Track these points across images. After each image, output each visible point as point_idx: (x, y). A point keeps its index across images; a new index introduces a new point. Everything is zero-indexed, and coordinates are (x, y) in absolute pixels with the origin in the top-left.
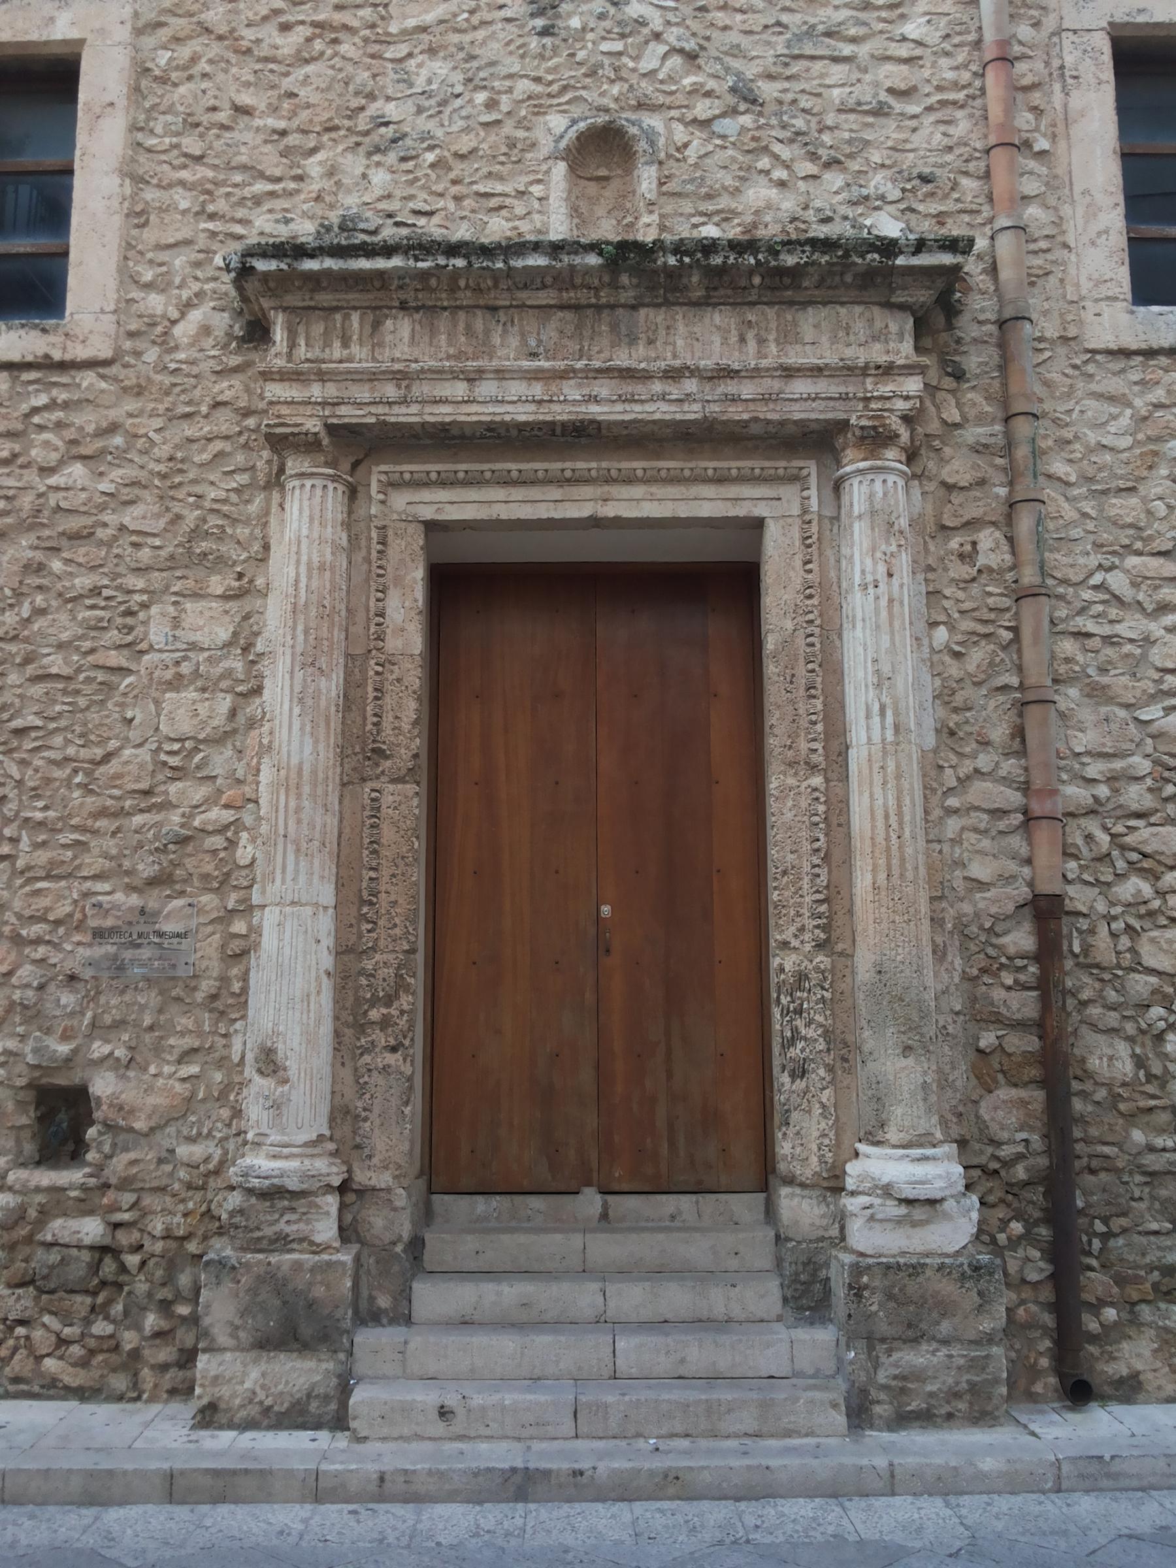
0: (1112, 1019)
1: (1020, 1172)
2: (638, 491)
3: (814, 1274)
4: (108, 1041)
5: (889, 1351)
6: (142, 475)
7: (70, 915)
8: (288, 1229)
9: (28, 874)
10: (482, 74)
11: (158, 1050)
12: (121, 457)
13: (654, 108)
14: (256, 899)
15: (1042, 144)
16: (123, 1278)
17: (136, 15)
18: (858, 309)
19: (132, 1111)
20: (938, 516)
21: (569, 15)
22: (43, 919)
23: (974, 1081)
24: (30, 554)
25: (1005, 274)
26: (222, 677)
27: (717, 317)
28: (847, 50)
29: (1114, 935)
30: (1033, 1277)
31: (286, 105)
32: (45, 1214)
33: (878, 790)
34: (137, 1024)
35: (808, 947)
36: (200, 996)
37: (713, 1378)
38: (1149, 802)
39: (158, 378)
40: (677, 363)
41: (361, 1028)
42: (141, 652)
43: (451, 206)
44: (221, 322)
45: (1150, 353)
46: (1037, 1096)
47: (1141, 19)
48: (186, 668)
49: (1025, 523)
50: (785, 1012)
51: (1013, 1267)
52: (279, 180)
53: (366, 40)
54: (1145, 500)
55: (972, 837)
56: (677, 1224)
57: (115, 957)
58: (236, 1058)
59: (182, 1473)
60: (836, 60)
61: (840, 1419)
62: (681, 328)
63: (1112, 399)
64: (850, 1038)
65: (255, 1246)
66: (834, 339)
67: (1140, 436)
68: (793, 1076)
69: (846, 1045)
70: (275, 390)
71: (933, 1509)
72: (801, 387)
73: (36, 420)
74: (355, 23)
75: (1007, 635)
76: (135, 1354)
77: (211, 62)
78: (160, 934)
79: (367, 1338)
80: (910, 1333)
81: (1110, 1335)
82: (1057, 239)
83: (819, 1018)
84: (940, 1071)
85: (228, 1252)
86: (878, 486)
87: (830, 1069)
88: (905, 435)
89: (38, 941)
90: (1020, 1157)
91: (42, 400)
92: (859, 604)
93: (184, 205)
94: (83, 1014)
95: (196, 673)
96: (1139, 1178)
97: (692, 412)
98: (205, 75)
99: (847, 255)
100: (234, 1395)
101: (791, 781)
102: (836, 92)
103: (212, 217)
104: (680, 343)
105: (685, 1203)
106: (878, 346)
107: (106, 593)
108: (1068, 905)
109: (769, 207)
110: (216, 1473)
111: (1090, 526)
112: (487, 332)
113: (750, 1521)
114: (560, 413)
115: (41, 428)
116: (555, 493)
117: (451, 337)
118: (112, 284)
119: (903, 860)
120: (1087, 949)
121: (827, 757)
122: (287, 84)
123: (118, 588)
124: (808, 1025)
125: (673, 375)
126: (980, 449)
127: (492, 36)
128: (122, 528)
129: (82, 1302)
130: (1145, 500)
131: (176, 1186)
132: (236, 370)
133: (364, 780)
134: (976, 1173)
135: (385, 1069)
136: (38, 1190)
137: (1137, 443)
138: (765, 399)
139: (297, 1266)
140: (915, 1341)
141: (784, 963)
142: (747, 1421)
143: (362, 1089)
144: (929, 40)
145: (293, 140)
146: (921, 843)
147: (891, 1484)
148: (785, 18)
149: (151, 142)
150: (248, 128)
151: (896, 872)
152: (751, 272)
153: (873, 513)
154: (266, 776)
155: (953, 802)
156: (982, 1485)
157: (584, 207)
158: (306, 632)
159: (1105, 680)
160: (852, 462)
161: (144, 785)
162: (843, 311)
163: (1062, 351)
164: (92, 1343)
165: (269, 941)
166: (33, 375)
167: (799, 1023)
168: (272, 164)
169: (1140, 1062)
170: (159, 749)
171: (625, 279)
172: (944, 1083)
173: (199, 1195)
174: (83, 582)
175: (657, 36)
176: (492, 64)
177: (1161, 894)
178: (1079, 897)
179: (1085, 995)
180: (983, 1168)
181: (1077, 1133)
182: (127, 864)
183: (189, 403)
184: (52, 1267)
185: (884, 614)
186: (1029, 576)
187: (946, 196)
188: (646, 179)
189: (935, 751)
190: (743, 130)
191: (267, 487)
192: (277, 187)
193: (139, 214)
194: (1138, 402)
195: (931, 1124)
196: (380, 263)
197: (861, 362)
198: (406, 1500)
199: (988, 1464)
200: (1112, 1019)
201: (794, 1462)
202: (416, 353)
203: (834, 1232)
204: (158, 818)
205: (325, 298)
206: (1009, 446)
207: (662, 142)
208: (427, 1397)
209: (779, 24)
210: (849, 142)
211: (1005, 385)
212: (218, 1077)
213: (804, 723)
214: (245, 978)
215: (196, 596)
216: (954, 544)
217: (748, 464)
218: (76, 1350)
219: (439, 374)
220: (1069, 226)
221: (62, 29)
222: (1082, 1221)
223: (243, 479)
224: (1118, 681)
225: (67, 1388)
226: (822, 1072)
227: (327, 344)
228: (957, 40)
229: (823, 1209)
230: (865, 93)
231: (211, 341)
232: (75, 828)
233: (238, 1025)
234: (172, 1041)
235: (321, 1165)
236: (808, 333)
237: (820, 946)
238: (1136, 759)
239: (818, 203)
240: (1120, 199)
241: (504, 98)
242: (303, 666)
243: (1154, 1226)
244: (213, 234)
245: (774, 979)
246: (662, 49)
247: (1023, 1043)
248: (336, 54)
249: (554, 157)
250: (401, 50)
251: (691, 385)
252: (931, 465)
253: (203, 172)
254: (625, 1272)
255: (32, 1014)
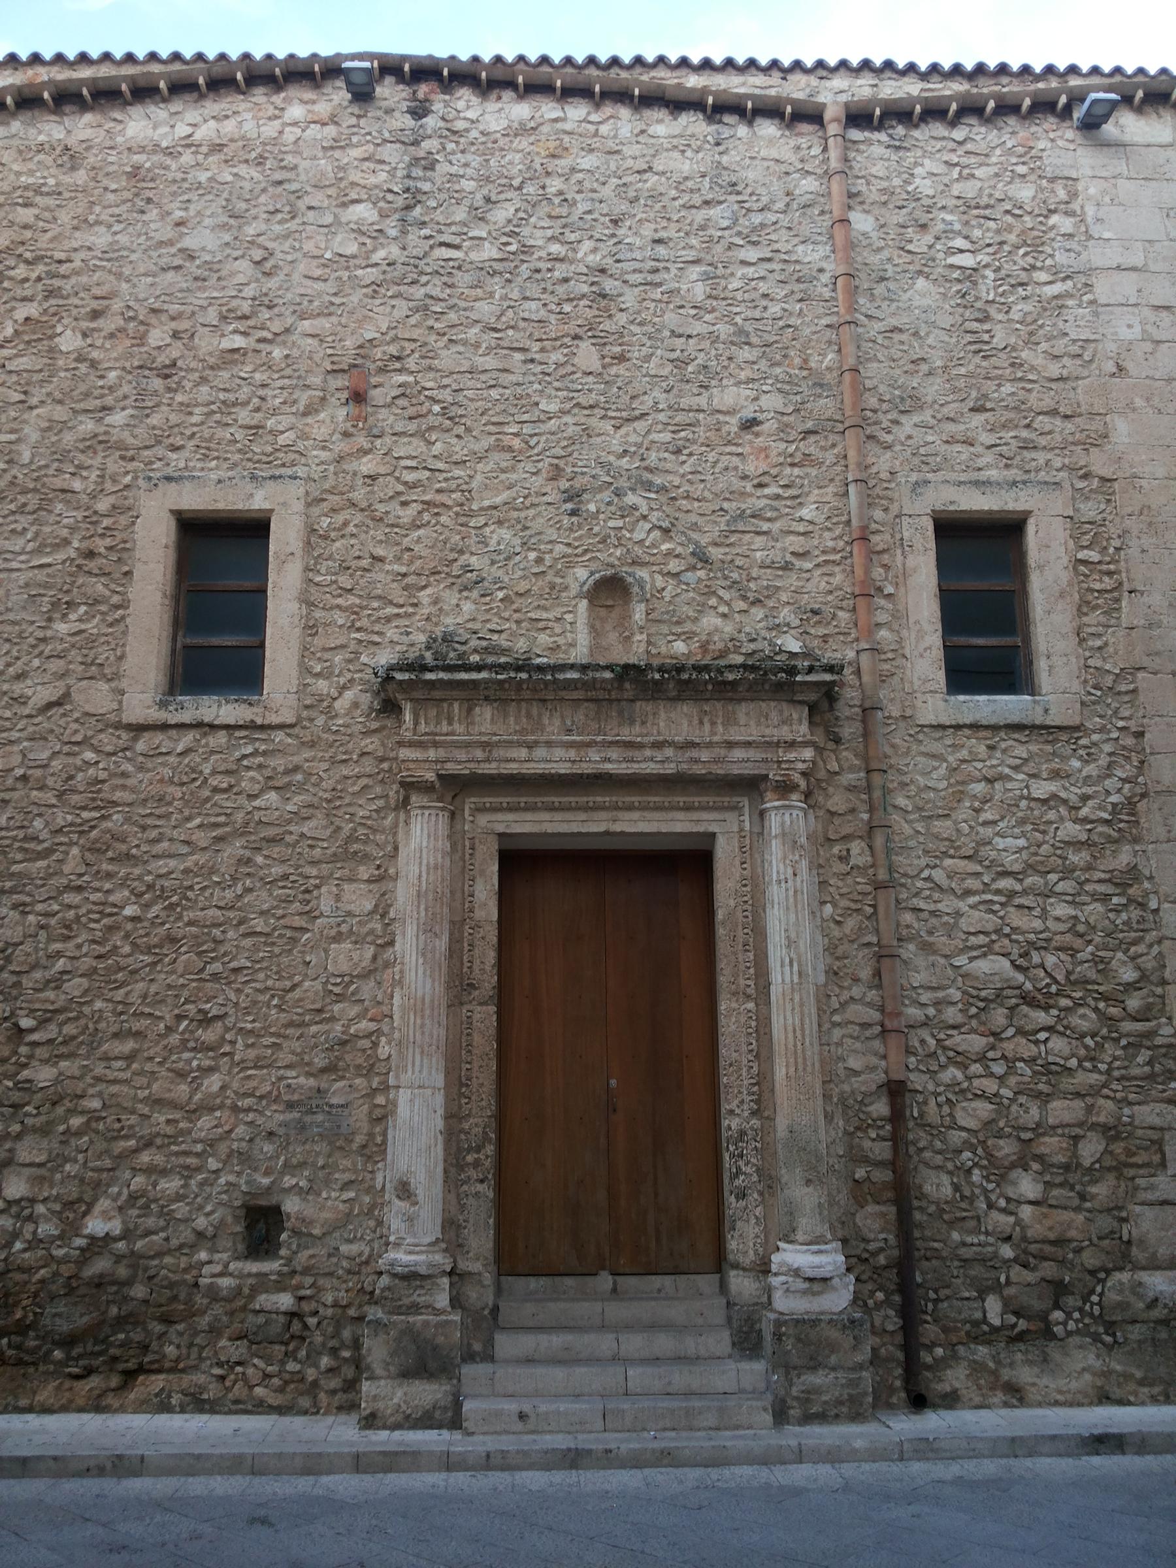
0: (939, 1159)
1: (882, 1260)
2: (635, 815)
3: (752, 1326)
4: (293, 1176)
5: (799, 1376)
6: (315, 800)
7: (270, 1093)
8: (419, 1300)
9: (243, 1065)
10: (533, 540)
11: (327, 1182)
12: (301, 788)
13: (644, 564)
14: (392, 1082)
15: (889, 589)
16: (306, 1333)
17: (307, 493)
18: (773, 704)
19: (311, 1222)
20: (826, 832)
21: (588, 502)
22: (252, 1095)
23: (852, 1201)
24: (242, 852)
25: (866, 678)
26: (368, 934)
27: (686, 708)
28: (765, 526)
29: (939, 1105)
30: (890, 1328)
31: (406, 556)
32: (254, 1291)
33: (789, 1013)
34: (314, 1164)
35: (746, 1114)
36: (355, 1146)
37: (689, 1394)
38: (960, 1019)
39: (325, 736)
40: (661, 738)
41: (461, 1168)
42: (316, 917)
43: (514, 627)
44: (366, 699)
45: (958, 727)
46: (893, 1209)
47: (952, 508)
48: (344, 928)
49: (879, 841)
50: (732, 1156)
51: (877, 1322)
52: (402, 606)
53: (457, 514)
54: (956, 823)
55: (849, 1041)
56: (662, 1295)
57: (300, 1121)
58: (379, 1187)
59: (364, 1454)
60: (758, 533)
61: (768, 1418)
62: (663, 715)
63: (934, 756)
64: (773, 1173)
65: (398, 1311)
66: (758, 724)
67: (952, 781)
68: (737, 1198)
69: (771, 1178)
70: (404, 753)
71: (825, 1470)
72: (738, 754)
73: (245, 763)
74: (450, 503)
75: (869, 910)
76: (315, 1384)
77: (356, 526)
78: (331, 1106)
79: (468, 1370)
80: (812, 1364)
81: (940, 1365)
82: (899, 652)
83: (754, 1160)
84: (829, 1195)
85: (380, 1315)
86: (787, 817)
87: (761, 1194)
88: (803, 784)
89: (249, 1110)
90: (882, 1250)
91: (249, 750)
92: (776, 893)
93: (340, 622)
94: (278, 1158)
95: (351, 932)
96: (956, 1263)
97: (670, 769)
98: (353, 535)
99: (765, 674)
100: (386, 1408)
101: (734, 1005)
102: (759, 554)
103: (359, 630)
104: (662, 724)
105: (667, 1281)
106: (786, 728)
107: (292, 878)
108: (910, 1086)
109: (716, 630)
110: (384, 1453)
111: (921, 839)
112: (540, 715)
113: (714, 1477)
114: (586, 769)
115: (248, 768)
116: (582, 816)
117: (517, 718)
118: (295, 673)
119: (805, 1059)
120: (922, 1115)
121: (757, 989)
122: (406, 542)
123: (300, 875)
124: (746, 1164)
125: (658, 745)
126: (851, 789)
127: (539, 514)
128: (302, 835)
129: (279, 1349)
130: (956, 823)
131: (340, 1272)
132: (375, 731)
133: (462, 1004)
134: (854, 1260)
135: (477, 1195)
136: (250, 1275)
137: (950, 785)
138: (716, 761)
139: (426, 1324)
140: (814, 1369)
141: (731, 1124)
142: (711, 1420)
143: (462, 1208)
144: (817, 520)
145: (411, 580)
146: (817, 1048)
147: (800, 1456)
148: (726, 505)
149: (318, 579)
150: (381, 570)
151: (800, 1068)
152: (706, 682)
153: (784, 834)
154: (397, 1001)
155: (837, 1018)
156: (854, 1456)
157: (598, 625)
158: (426, 910)
159: (931, 939)
160: (771, 801)
161: (318, 1006)
162: (763, 705)
163: (902, 724)
164: (287, 1376)
165: (403, 1110)
166: (243, 733)
167: (741, 1163)
168: (398, 595)
169: (956, 1188)
170: (327, 982)
171: (627, 685)
172: (832, 1202)
173: (356, 1278)
174: (277, 870)
175: (645, 517)
176: (540, 533)
177: (969, 1078)
178: (917, 1081)
179: (921, 1145)
180: (859, 1258)
181: (917, 1234)
182: (307, 1058)
183: (345, 753)
184: (259, 1327)
185: (791, 900)
186: (882, 875)
187: (829, 623)
188: (639, 613)
189: (826, 985)
190: (700, 580)
191: (396, 809)
192: (401, 611)
193: (311, 627)
194: (951, 759)
195: (824, 1230)
196: (474, 676)
197: (775, 739)
198: (503, 1469)
199: (858, 1444)
200: (939, 1159)
201: (740, 1444)
202: (495, 729)
203: (765, 1299)
204: (327, 1027)
205: (437, 694)
206: (869, 788)
207: (648, 587)
208: (512, 1407)
209: (722, 509)
210: (767, 588)
211: (866, 747)
212: (367, 1199)
213: (742, 967)
214: (384, 1134)
215: (351, 880)
216: (836, 850)
217: (706, 799)
218: (276, 1381)
219: (510, 744)
220: (907, 644)
221: (258, 500)
222: (921, 1291)
223: (380, 803)
224: (940, 939)
225: (270, 1406)
226: (756, 1195)
227: (438, 723)
228: (835, 520)
229: (757, 1285)
230: (776, 556)
231: (359, 712)
232: (273, 1034)
233: (380, 1165)
234: (337, 1176)
235: (438, 1258)
236: (742, 719)
237: (754, 1113)
238: (951, 991)
239: (747, 629)
240: (939, 626)
241: (547, 556)
242: (425, 932)
243: (967, 1294)
244: (360, 641)
245: (724, 1134)
246: (648, 526)
247: (883, 1176)
248: (438, 523)
249: (579, 596)
250: (481, 521)
251: (669, 752)
252: (820, 799)
253: (353, 600)
254: (630, 1327)
255: (245, 1158)
